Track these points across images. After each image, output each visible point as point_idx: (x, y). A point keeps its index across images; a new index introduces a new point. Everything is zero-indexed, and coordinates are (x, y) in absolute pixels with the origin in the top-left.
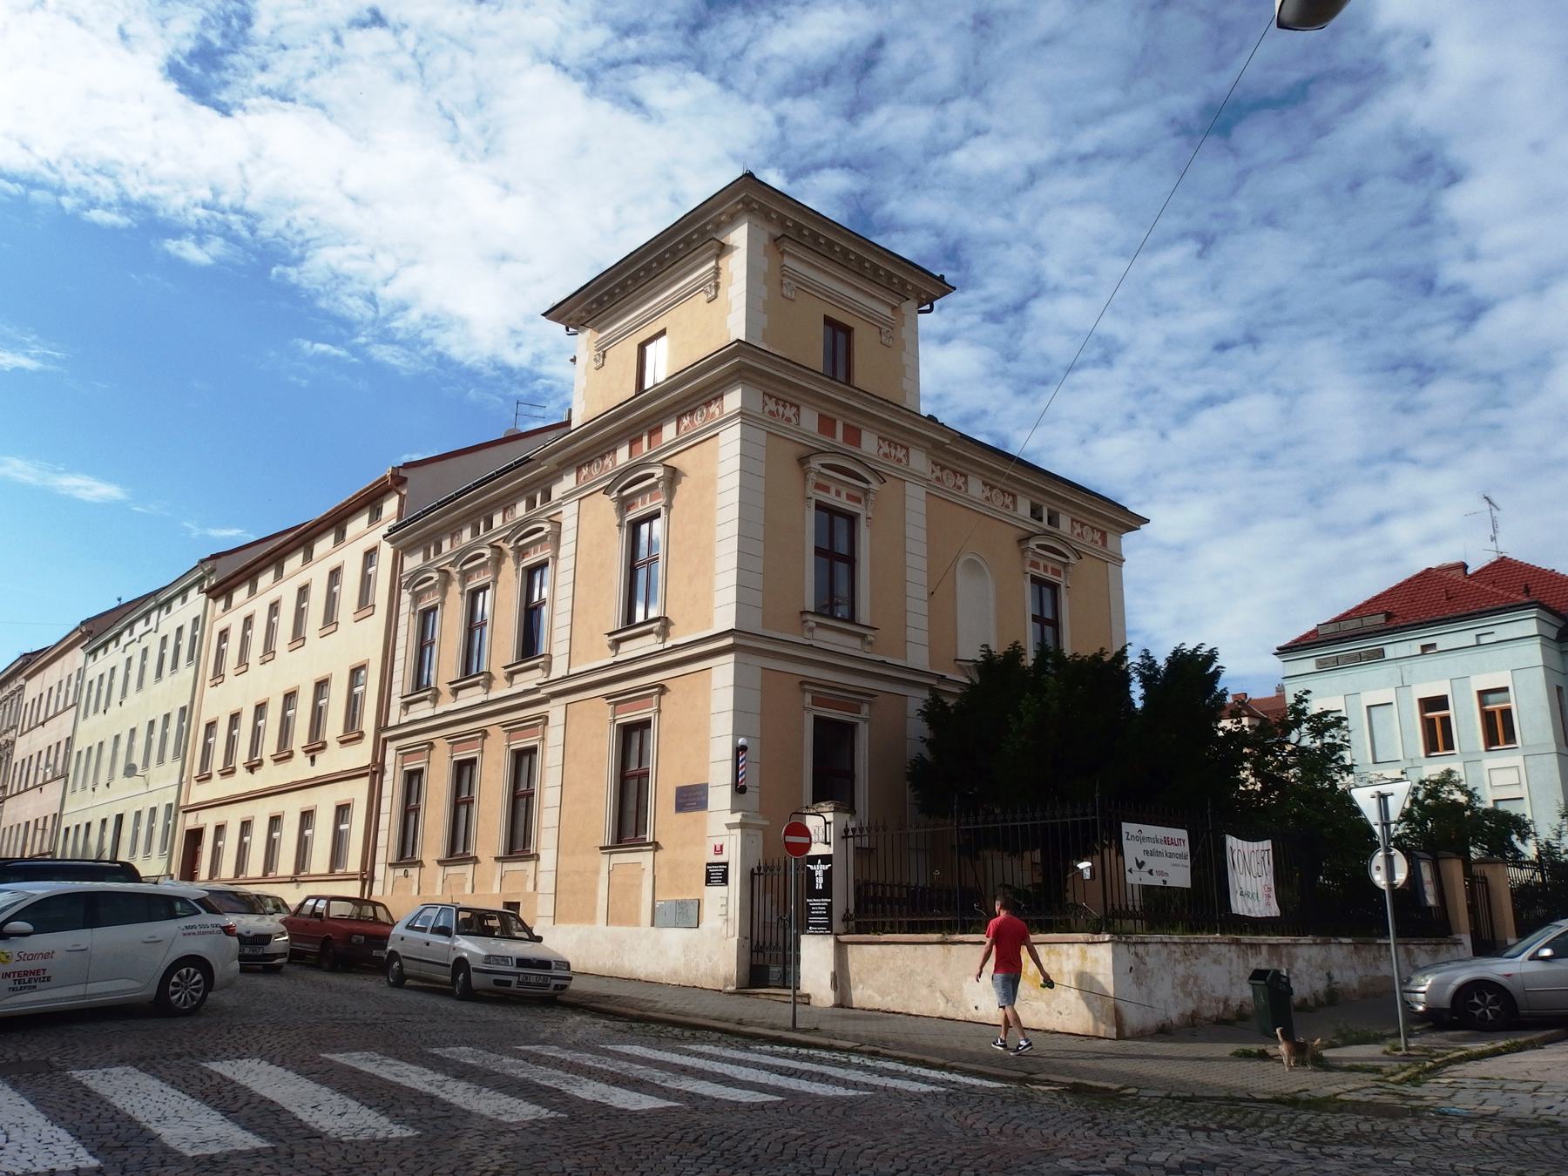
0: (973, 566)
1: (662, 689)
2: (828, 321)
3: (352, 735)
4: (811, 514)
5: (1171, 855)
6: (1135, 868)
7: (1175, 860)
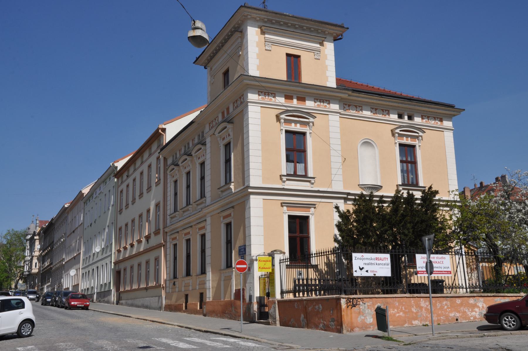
0: (367, 143)
1: (314, 205)
2: (288, 55)
3: (157, 233)
4: (283, 136)
5: (379, 264)
6: (358, 270)
7: (381, 266)
